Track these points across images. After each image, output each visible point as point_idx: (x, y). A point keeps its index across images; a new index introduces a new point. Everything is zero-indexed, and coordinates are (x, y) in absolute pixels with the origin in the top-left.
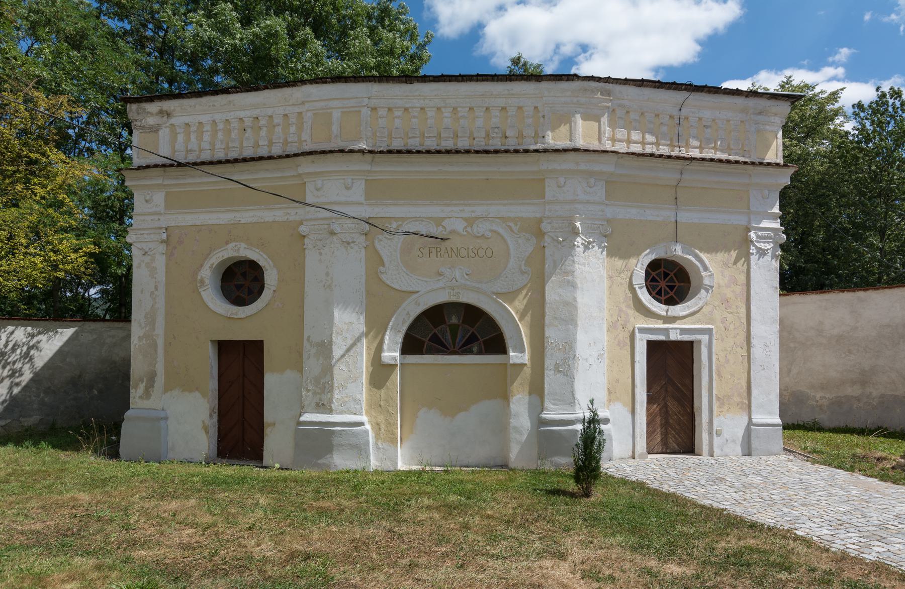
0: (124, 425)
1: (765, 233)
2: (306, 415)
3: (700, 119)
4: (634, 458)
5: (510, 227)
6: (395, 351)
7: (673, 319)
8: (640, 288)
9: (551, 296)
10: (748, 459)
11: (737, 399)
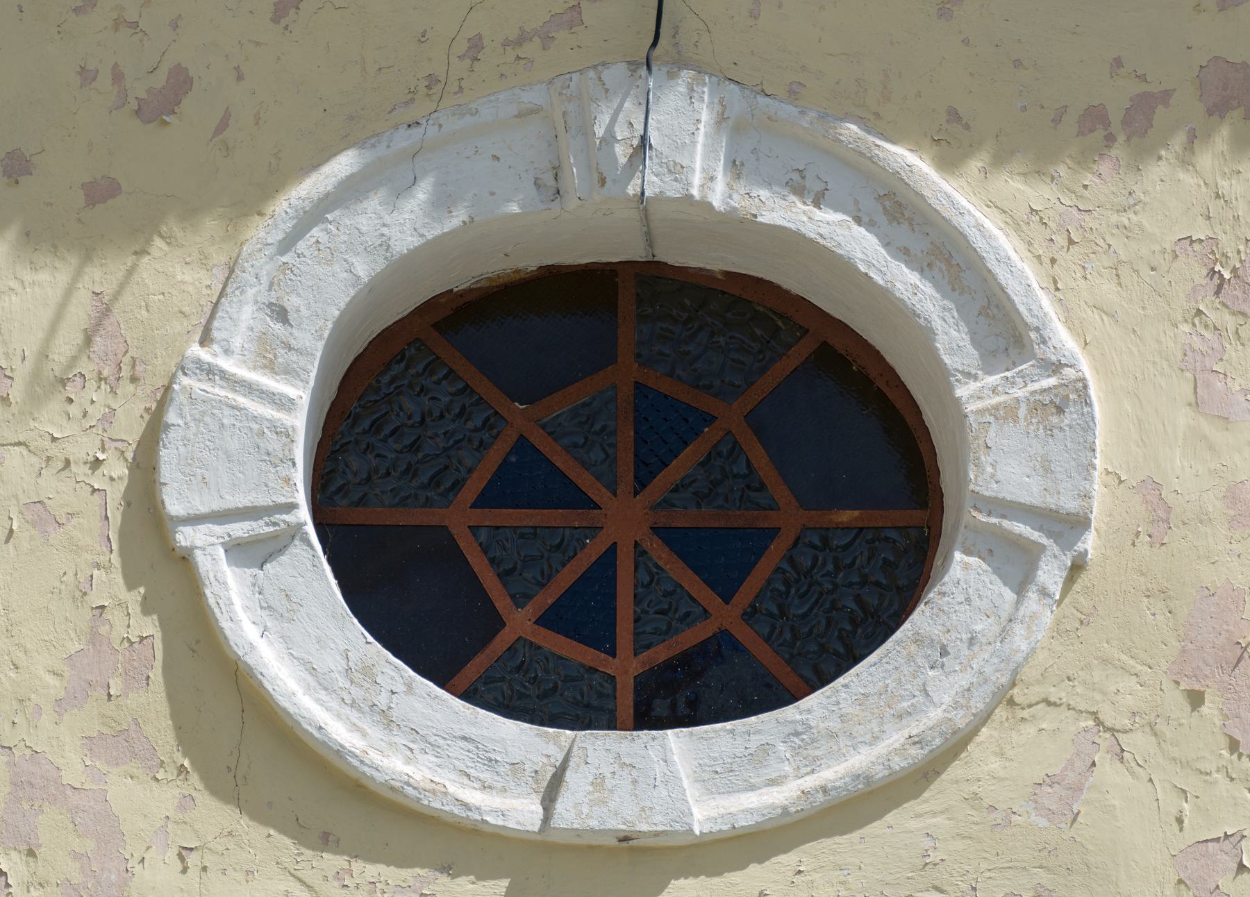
2: (596, 128)
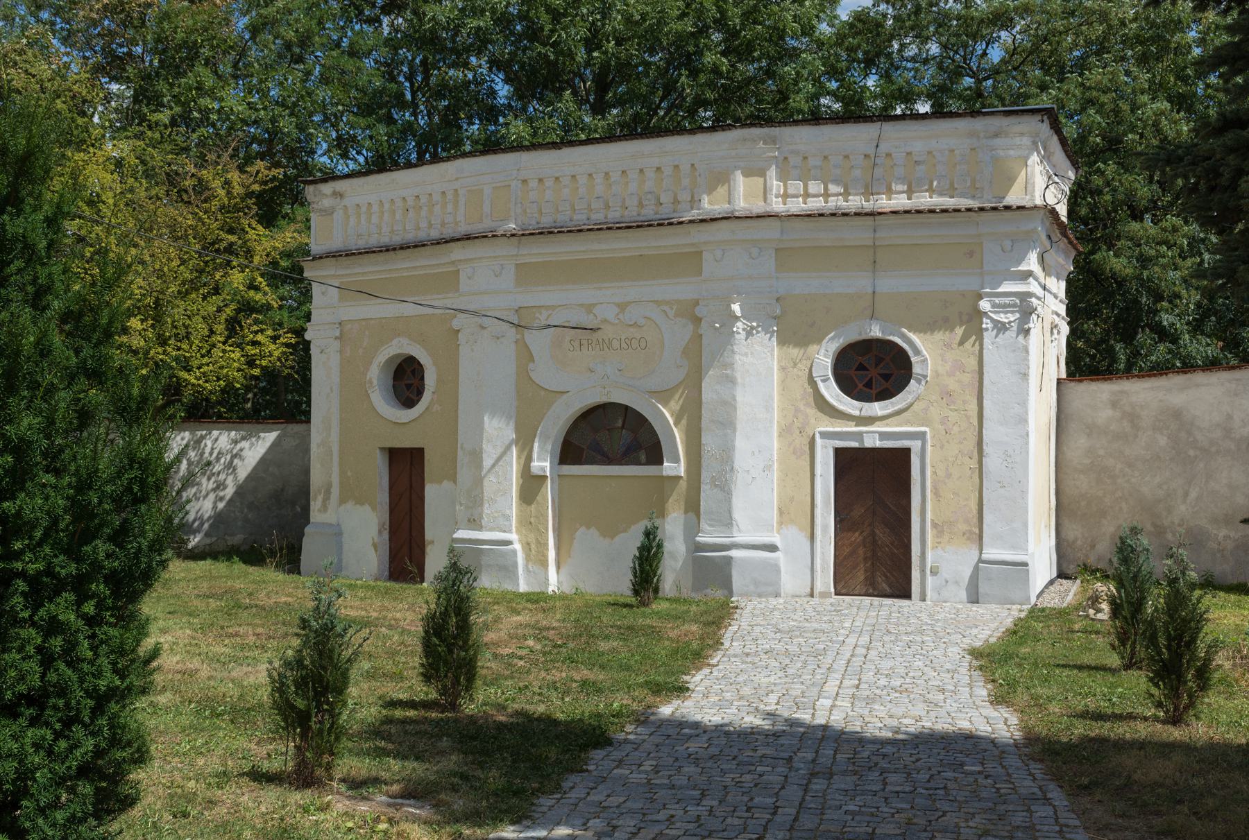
0: (304, 539)
1: (1007, 300)
3: (909, 154)
4: (812, 595)
5: (665, 311)
6: (545, 460)
7: (870, 420)
10: (975, 607)
11: (962, 527)
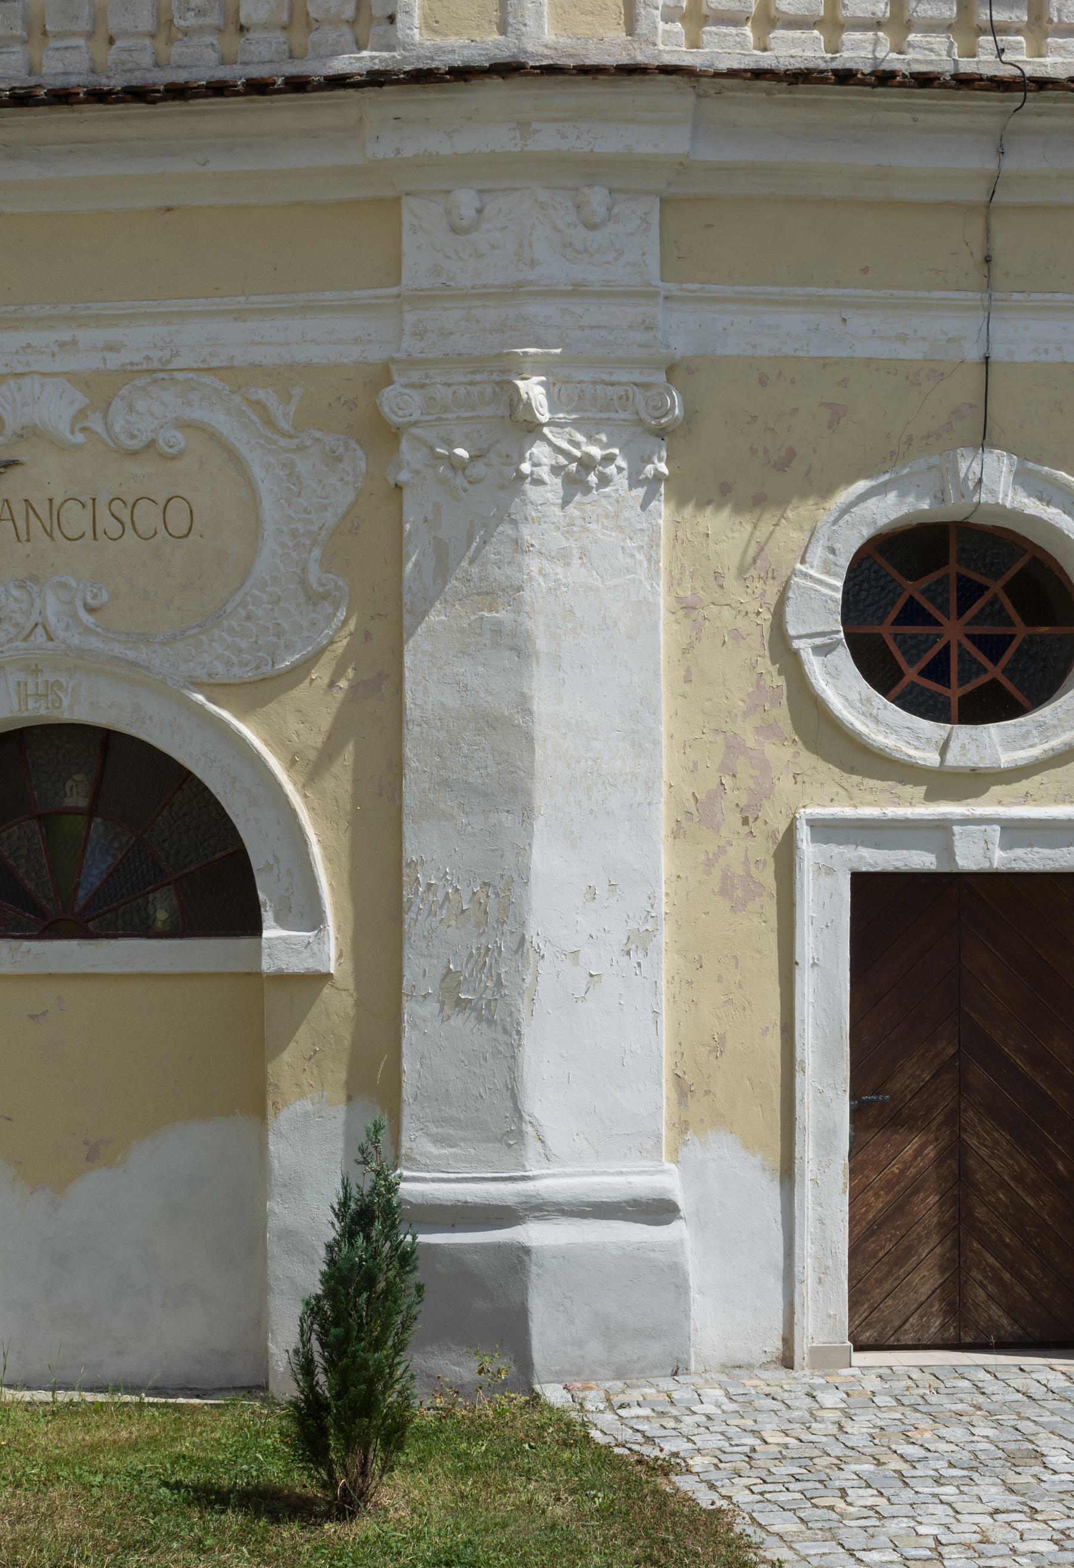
4: (787, 1362)
5: (260, 406)
8: (822, 651)
9: (426, 691)
